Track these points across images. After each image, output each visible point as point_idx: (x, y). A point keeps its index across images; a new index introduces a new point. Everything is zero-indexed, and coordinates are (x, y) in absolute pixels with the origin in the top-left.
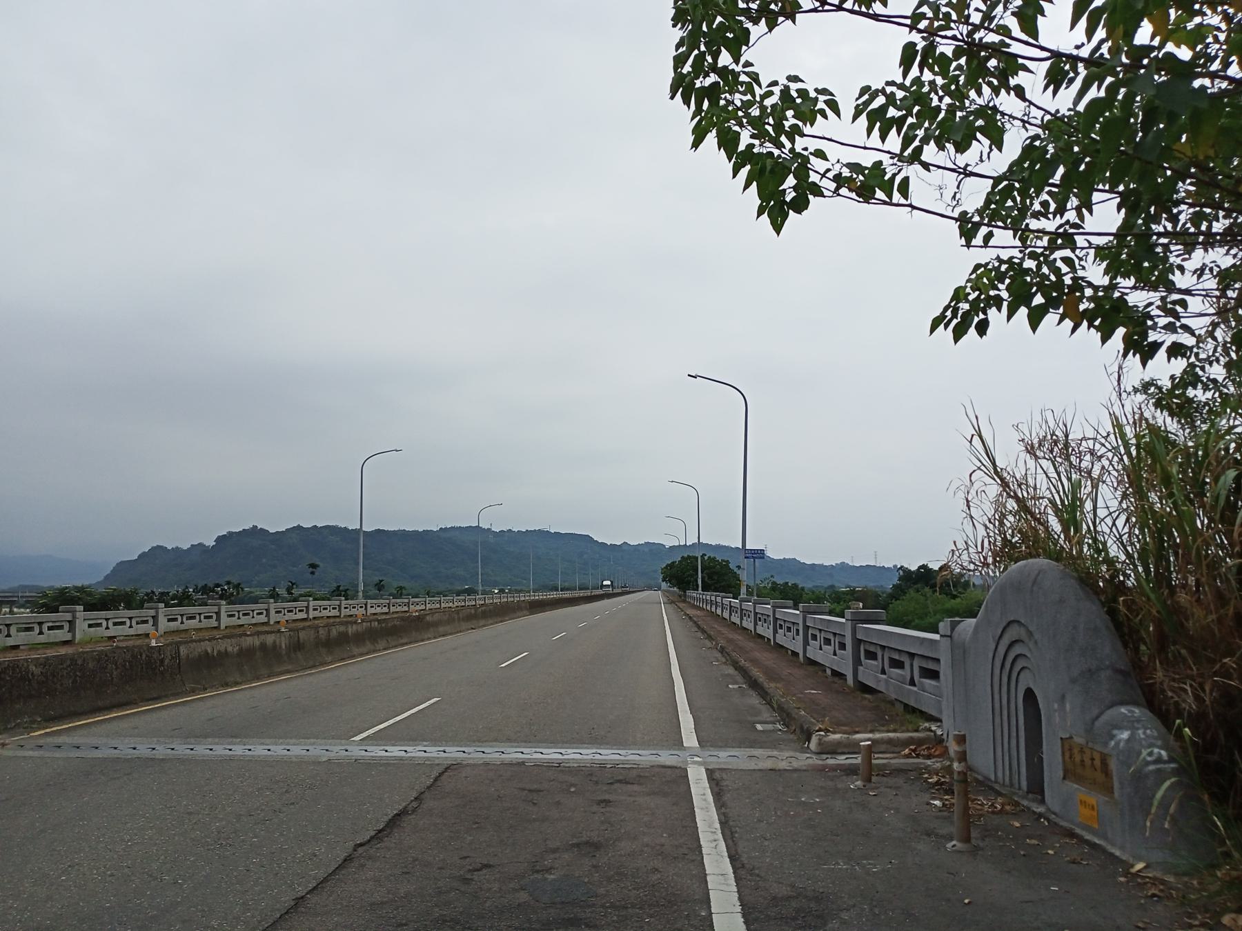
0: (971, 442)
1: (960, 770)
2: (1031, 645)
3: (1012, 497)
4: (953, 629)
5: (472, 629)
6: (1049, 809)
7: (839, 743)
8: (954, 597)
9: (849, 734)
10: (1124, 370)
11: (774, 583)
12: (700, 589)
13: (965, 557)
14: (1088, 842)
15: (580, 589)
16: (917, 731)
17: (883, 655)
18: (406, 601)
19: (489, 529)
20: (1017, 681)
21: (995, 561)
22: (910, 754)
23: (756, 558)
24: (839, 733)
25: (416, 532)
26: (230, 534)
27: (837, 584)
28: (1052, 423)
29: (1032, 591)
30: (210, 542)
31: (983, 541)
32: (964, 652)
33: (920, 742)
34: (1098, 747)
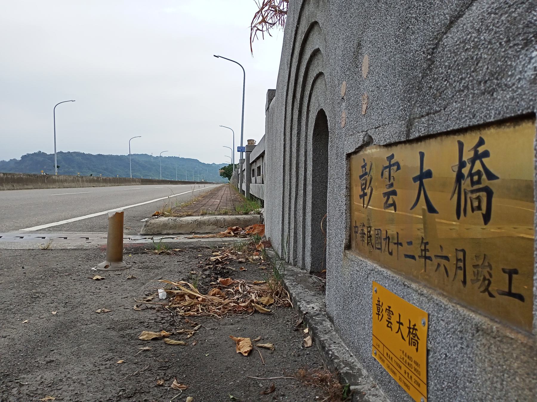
7: (165, 225)
22: (229, 233)
25: (117, 156)
26: (28, 155)
30: (19, 158)
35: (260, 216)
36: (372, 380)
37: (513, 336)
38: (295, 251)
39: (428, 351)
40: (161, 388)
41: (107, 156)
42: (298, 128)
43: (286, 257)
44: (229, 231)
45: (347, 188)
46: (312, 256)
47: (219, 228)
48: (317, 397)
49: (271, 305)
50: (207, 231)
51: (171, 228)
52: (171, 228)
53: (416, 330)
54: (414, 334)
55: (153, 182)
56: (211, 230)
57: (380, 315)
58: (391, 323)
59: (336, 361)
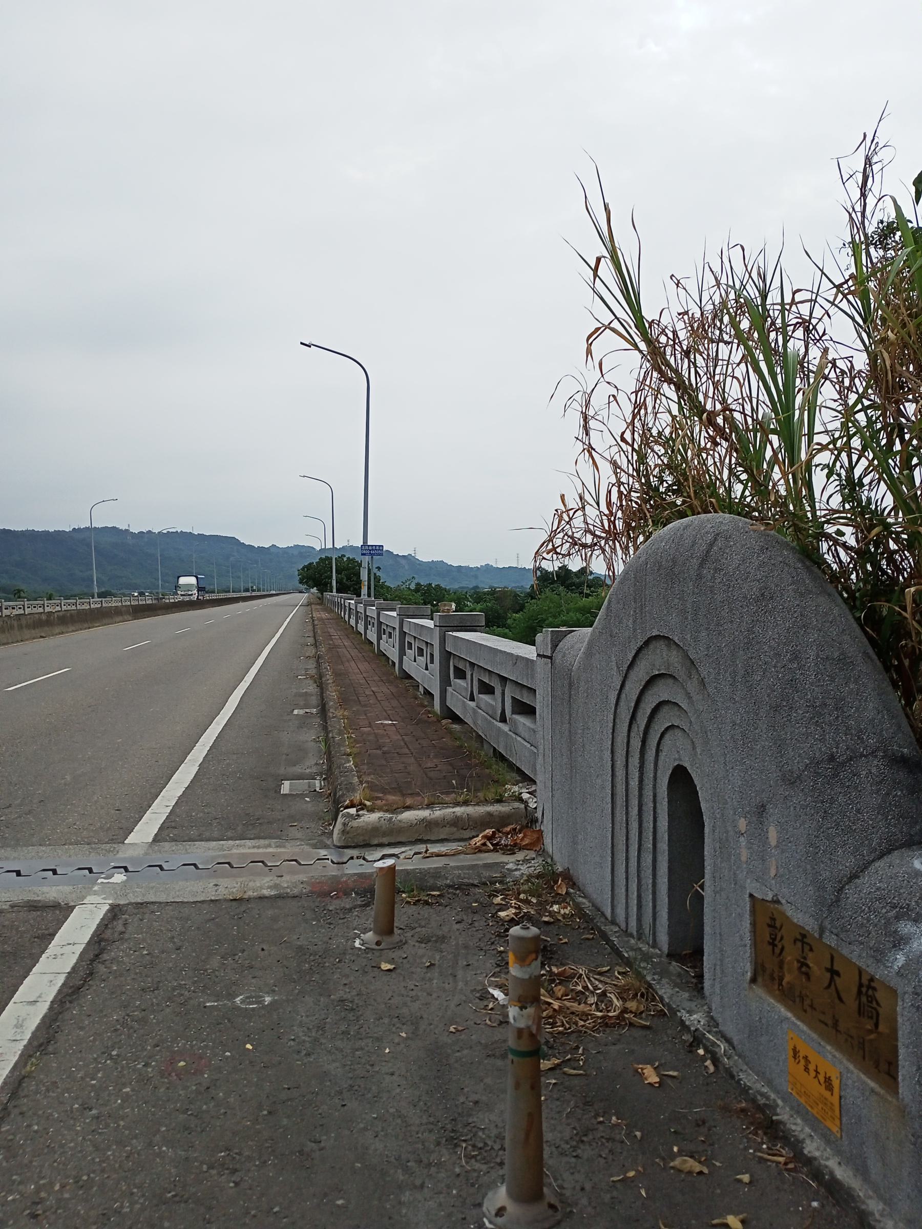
0: (595, 270)
1: (522, 1024)
2: (692, 686)
3: (670, 381)
4: (555, 646)
5: (42, 637)
6: (713, 1022)
7: (375, 830)
8: (587, 596)
9: (394, 811)
10: (876, 168)
11: (418, 584)
12: (335, 590)
13: (578, 522)
14: (818, 1174)
15: (244, 591)
16: (499, 801)
17: (472, 675)
19: (127, 530)
21: (627, 525)
22: (484, 844)
23: (374, 555)
24: (380, 809)
25: (47, 533)
27: (481, 585)
28: (739, 269)
29: (700, 576)
31: (609, 492)
32: (571, 685)
34: (857, 955)
37: (890, 1099)
39: (840, 1097)
41: (23, 533)
44: (483, 841)
45: (751, 924)
49: (642, 1013)
50: (442, 837)
51: (384, 834)
52: (384, 834)
53: (874, 989)
54: (870, 996)
57: (776, 946)
58: (808, 966)
59: (751, 1091)
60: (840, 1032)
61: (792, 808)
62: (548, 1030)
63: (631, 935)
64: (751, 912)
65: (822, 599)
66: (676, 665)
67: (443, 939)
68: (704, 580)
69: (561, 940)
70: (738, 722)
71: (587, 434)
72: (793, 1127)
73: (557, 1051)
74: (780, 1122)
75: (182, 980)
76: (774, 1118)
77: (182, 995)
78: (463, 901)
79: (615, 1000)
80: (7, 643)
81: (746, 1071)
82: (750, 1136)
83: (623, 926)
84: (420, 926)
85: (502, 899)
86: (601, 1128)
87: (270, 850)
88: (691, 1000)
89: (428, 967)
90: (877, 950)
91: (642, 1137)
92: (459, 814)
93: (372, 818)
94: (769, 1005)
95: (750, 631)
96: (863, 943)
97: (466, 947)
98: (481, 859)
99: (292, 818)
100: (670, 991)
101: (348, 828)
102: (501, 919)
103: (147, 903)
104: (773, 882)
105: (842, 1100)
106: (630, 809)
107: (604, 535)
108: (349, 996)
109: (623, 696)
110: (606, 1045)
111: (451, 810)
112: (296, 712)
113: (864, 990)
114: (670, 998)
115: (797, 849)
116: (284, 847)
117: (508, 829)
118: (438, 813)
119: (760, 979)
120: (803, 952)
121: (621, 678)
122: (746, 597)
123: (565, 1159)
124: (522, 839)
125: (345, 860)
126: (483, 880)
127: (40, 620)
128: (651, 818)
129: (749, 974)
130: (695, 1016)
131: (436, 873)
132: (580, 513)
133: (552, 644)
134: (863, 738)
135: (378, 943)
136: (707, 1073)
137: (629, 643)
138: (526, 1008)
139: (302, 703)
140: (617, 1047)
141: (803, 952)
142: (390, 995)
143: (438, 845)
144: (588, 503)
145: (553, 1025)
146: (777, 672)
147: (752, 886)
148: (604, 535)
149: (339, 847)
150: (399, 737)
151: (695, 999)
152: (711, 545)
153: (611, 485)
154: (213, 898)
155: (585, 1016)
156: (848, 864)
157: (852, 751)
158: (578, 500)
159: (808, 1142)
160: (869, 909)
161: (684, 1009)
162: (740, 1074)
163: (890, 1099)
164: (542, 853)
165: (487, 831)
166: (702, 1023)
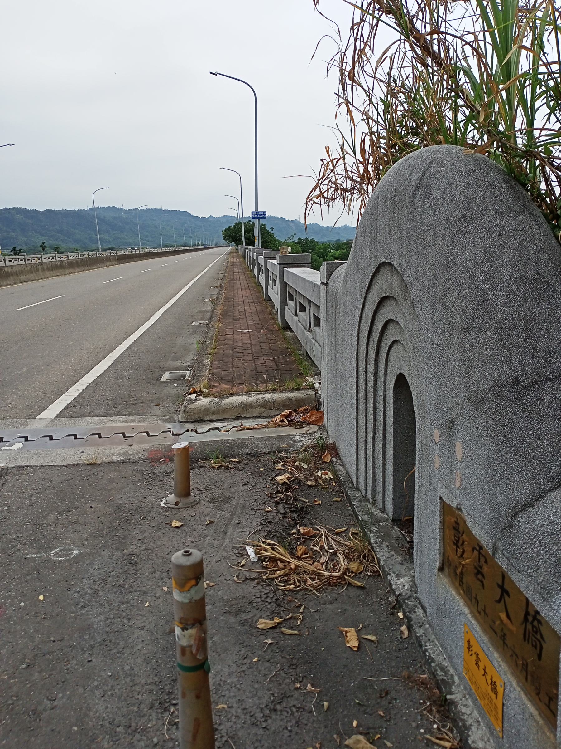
4: (329, 275)
7: (207, 410)
11: (300, 239)
12: (244, 244)
13: (340, 169)
16: (298, 389)
18: (40, 256)
19: (122, 209)
20: (387, 360)
22: (282, 421)
23: (260, 218)
24: (213, 395)
25: (74, 211)
31: (363, 141)
32: (336, 306)
33: (300, 403)
35: (315, 394)
36: (462, 688)
38: (374, 490)
39: (503, 705)
40: (299, 691)
42: (375, 367)
43: (362, 487)
44: (281, 419)
45: (440, 522)
46: (394, 505)
47: (269, 411)
48: (421, 701)
51: (214, 413)
52: (214, 413)
55: (133, 258)
56: (259, 413)
59: (433, 665)
60: (507, 645)
61: (475, 429)
62: (281, 588)
63: (368, 501)
64: (440, 512)
65: (522, 218)
66: (396, 289)
67: (228, 499)
68: (416, 206)
69: (316, 501)
70: (436, 341)
71: (343, 89)
72: (464, 710)
73: (283, 609)
74: (452, 702)
75: (20, 533)
76: (448, 697)
77: (14, 547)
78: (255, 466)
79: (342, 561)
80: (36, 280)
81: (433, 641)
82: (425, 712)
83: (363, 493)
84: (215, 488)
85: (282, 466)
86: (296, 694)
87: (133, 424)
88: (402, 564)
89: (207, 524)
90: (544, 588)
91: (328, 708)
92: (267, 399)
93: (204, 401)
94: (451, 595)
95: (450, 253)
96: (532, 576)
97: (243, 507)
98: (277, 433)
99: (159, 399)
100: (387, 554)
101: (188, 409)
102: (277, 483)
103: (28, 466)
104: (458, 492)
105: (505, 708)
106: (368, 405)
107: (358, 179)
108: (137, 551)
109: (364, 315)
110: (324, 604)
111: (262, 396)
112: (194, 323)
113: (530, 618)
114: (385, 561)
115: (478, 468)
116: (144, 421)
117: (302, 409)
118: (252, 398)
119: (446, 570)
120: (479, 561)
121: (362, 300)
122: (448, 220)
123: (254, 730)
124: (310, 417)
125: (182, 432)
126: (274, 449)
127: (56, 265)
128: (382, 414)
129: (438, 563)
130: (402, 580)
131: (241, 444)
132: (341, 162)
133: (327, 273)
134: (550, 360)
135: (176, 504)
136: (401, 638)
137: (367, 270)
138: (187, 629)
139: (200, 317)
140: (335, 605)
141: (479, 561)
142: (170, 550)
143: (251, 420)
144: (347, 153)
145: (286, 582)
146: (470, 293)
147: (442, 492)
148: (358, 179)
149: (181, 422)
150: (249, 341)
151: (405, 563)
152: (424, 173)
153: (364, 135)
154: (76, 463)
155: (315, 574)
156: (523, 492)
157: (538, 374)
158: (340, 151)
159: (474, 728)
160: (540, 542)
161: (394, 573)
162: (427, 644)
163: (548, 734)
164: (323, 428)
165: (286, 411)
166: (406, 588)
